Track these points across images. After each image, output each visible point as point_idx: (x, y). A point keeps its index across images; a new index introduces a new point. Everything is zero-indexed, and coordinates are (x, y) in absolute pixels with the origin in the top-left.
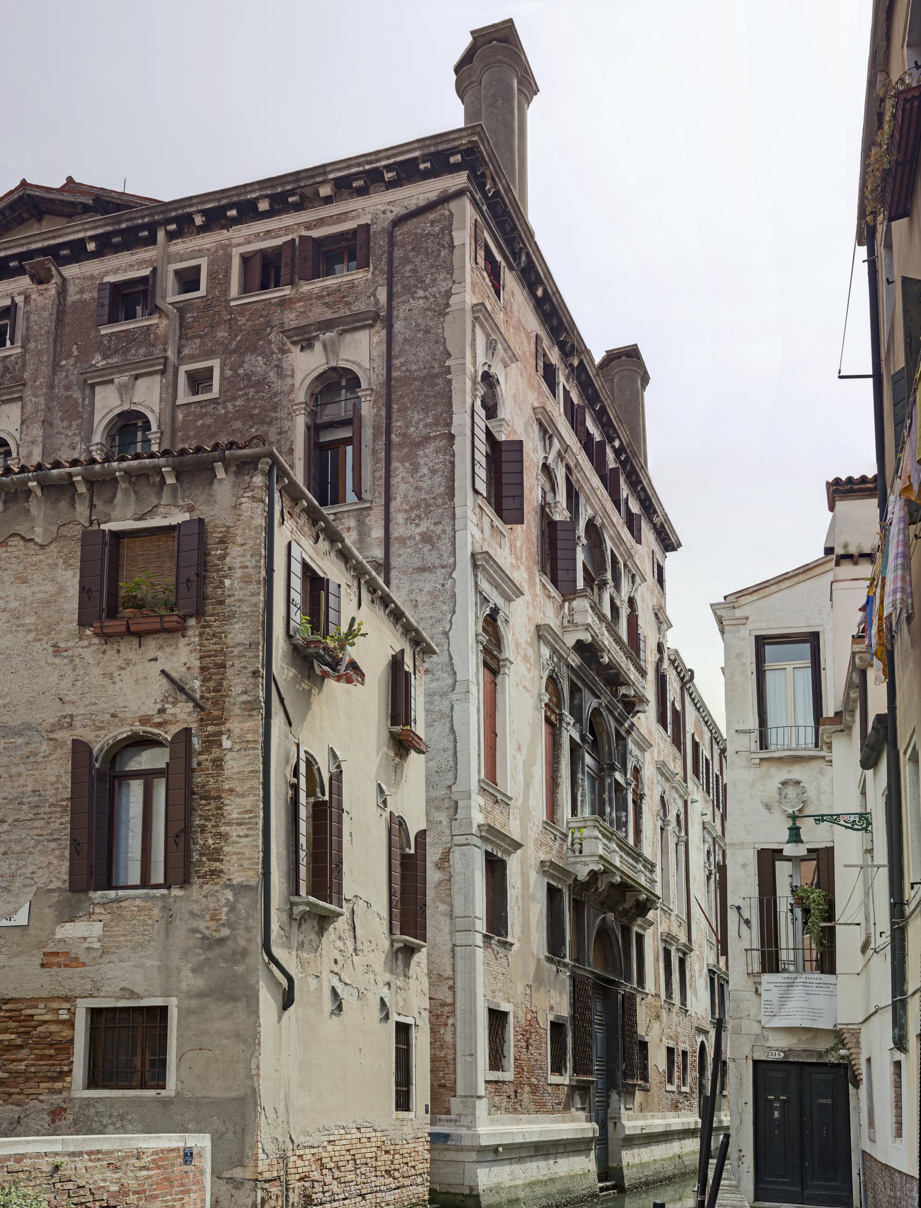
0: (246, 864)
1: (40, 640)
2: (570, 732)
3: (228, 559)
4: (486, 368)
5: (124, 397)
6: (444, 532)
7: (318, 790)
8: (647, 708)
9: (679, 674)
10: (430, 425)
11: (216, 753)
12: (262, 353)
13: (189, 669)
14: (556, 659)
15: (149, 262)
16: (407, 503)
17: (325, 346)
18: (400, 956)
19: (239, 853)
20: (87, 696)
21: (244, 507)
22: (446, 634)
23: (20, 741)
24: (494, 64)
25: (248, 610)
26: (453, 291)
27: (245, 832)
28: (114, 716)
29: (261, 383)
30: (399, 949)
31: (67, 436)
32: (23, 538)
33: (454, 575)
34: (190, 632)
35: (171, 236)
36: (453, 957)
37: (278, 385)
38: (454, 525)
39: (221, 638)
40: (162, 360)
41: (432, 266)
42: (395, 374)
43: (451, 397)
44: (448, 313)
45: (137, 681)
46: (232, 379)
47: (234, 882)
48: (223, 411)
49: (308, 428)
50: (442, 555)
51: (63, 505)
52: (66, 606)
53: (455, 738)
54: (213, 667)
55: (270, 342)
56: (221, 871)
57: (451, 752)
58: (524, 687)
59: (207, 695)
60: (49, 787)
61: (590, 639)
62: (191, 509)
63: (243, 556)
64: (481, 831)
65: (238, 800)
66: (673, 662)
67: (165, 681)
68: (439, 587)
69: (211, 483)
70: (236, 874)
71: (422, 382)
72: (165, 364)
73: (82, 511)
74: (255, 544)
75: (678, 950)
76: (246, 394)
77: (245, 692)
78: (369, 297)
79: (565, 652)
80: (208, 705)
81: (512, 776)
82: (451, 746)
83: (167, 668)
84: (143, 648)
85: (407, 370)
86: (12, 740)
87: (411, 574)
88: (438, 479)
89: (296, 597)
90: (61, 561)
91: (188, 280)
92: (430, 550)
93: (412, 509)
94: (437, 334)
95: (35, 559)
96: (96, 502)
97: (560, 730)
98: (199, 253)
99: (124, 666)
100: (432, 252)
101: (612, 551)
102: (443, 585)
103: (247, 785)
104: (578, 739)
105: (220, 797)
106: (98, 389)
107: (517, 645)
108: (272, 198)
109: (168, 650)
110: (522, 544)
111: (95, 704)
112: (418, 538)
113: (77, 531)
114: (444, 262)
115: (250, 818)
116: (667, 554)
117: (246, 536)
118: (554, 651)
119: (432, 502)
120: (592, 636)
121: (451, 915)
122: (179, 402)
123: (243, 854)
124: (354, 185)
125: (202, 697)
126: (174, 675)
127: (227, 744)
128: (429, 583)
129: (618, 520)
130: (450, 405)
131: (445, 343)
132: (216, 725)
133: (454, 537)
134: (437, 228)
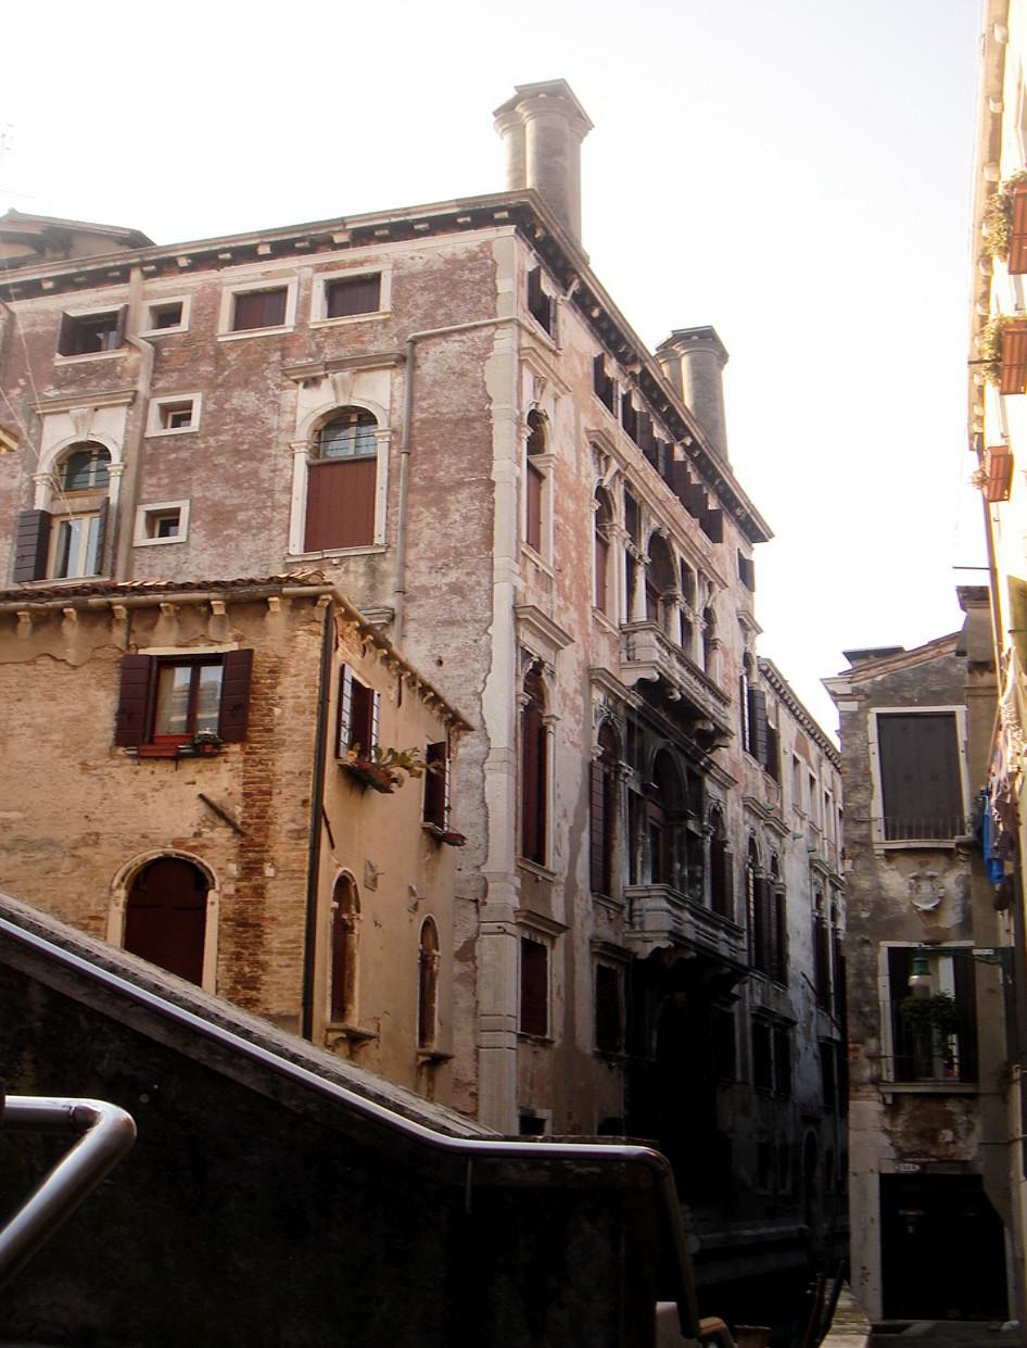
0: (287, 994)
1: (66, 757)
2: (630, 781)
3: (279, 689)
4: (533, 407)
5: (81, 428)
6: (479, 583)
7: (353, 907)
8: (730, 742)
9: (773, 685)
10: (464, 469)
11: (257, 880)
12: (257, 390)
13: (230, 794)
14: (611, 702)
15: (122, 299)
16: (433, 550)
17: (335, 385)
18: (425, 1070)
19: (278, 983)
20: (117, 814)
21: (299, 639)
22: (478, 695)
23: (40, 855)
24: (550, 117)
25: (299, 739)
26: (496, 337)
27: (288, 962)
28: (144, 836)
29: (255, 418)
30: (424, 1063)
31: (6, 464)
32: (54, 658)
33: (489, 631)
34: (232, 758)
35: (148, 276)
36: (477, 1059)
37: (274, 421)
38: (492, 576)
39: (267, 765)
40: (131, 394)
41: (469, 311)
42: (418, 415)
43: (491, 442)
44: (489, 358)
45: (171, 804)
46: (216, 413)
47: (272, 1012)
48: (203, 446)
49: (310, 467)
50: (475, 609)
51: (100, 629)
52: (97, 726)
53: (487, 813)
54: (258, 794)
55: (266, 378)
56: (258, 1000)
57: (480, 828)
58: (572, 742)
59: (250, 821)
60: (69, 904)
61: (657, 677)
62: (238, 639)
63: (296, 686)
64: (517, 917)
65: (281, 930)
66: (764, 673)
67: (202, 805)
68: (471, 642)
69: (264, 616)
70: (275, 1004)
71: (456, 425)
72: (134, 398)
73: (119, 634)
74: (310, 676)
75: (776, 1025)
76: (232, 429)
77: (293, 821)
78: (392, 338)
79: (624, 694)
80: (250, 832)
81: (556, 848)
82: (481, 821)
83: (207, 792)
84: (179, 771)
85: (437, 412)
86: (32, 854)
87: (435, 626)
88: (472, 526)
89: (346, 718)
90: (93, 681)
91: (167, 316)
92: (459, 603)
93: (438, 557)
94: (475, 378)
95: (65, 678)
96: (134, 627)
97: (615, 782)
98: (183, 291)
99: (158, 787)
100: (471, 298)
101: (682, 560)
102: (475, 641)
103: (291, 914)
104: (637, 790)
105: (259, 925)
106: (48, 420)
107: (565, 695)
108: (274, 245)
109: (209, 774)
110: (572, 583)
111: (125, 824)
112: (445, 588)
113: (111, 654)
114: (485, 308)
115: (293, 948)
116: (754, 545)
117: (301, 667)
118: (610, 693)
119: (464, 550)
120: (659, 673)
121: (475, 1013)
122: (147, 435)
123: (283, 984)
124: (376, 234)
125: (243, 823)
126: (213, 799)
127: (269, 872)
128: (457, 639)
129: (689, 523)
130: (490, 450)
131: (484, 387)
132: (257, 852)
133: (492, 589)
134: (478, 277)
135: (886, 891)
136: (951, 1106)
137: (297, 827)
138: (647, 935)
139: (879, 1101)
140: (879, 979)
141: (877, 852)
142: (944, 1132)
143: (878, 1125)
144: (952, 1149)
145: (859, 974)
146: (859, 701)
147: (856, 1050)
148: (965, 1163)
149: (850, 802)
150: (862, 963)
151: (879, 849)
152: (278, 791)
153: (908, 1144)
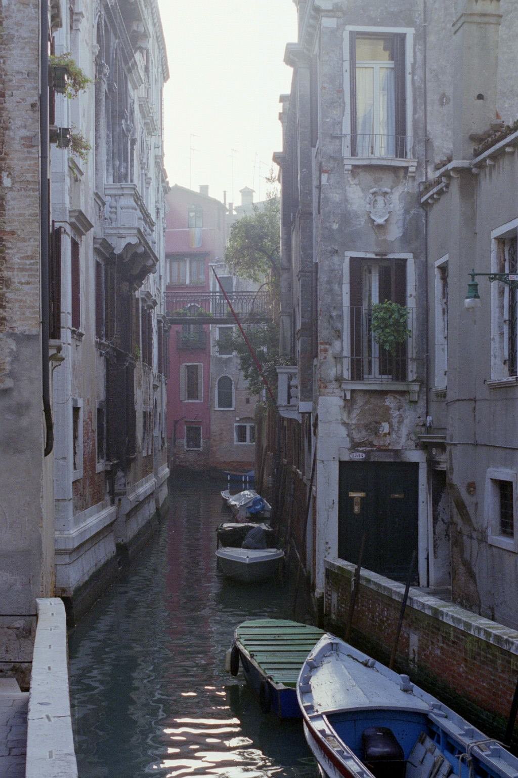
19: (21, 301)
25: (25, 35)
65: (19, 245)
77: (25, 127)
115: (31, 264)
135: (351, 204)
136: (390, 402)
137: (28, 134)
138: (121, 231)
139: (341, 397)
140: (343, 285)
141: (346, 167)
142: (383, 424)
143: (339, 418)
144: (388, 440)
145: (329, 282)
146: (338, 18)
147: (326, 350)
148: (397, 452)
149: (327, 118)
150: (332, 270)
151: (349, 163)
152: (10, 92)
153: (359, 435)
